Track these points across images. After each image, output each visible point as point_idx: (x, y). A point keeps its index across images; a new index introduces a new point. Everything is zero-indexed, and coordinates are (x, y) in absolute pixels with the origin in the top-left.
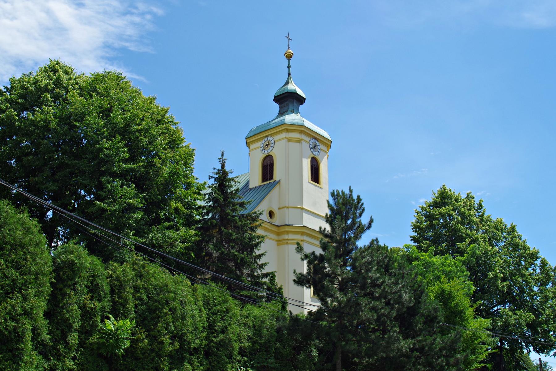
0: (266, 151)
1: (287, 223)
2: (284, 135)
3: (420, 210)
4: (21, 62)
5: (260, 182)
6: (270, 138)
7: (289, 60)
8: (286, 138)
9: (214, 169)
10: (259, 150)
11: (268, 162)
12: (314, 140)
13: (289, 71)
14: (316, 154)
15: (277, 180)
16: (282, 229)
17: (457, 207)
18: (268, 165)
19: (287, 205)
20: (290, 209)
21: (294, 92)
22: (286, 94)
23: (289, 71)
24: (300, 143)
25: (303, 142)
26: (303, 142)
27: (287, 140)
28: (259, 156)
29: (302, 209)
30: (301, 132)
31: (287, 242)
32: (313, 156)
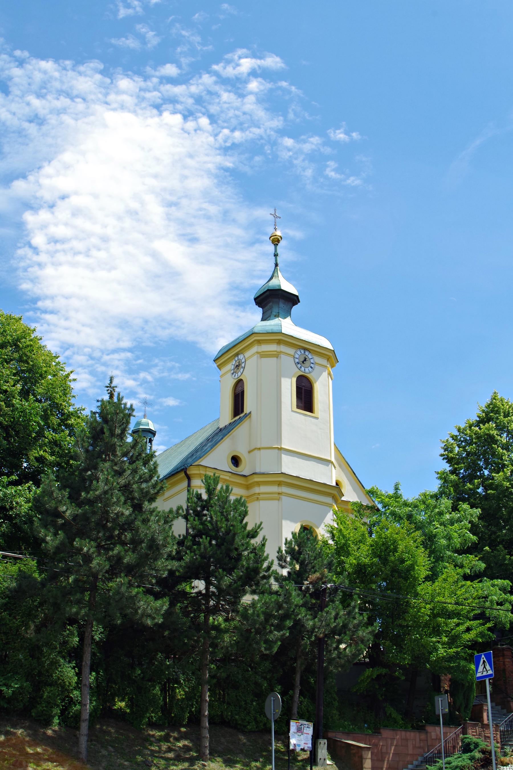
0: (237, 375)
1: (258, 471)
2: (255, 349)
3: (456, 433)
4: (128, 322)
5: (230, 419)
6: (241, 357)
7: (276, 245)
8: (257, 353)
9: (98, 401)
10: (229, 374)
11: (239, 389)
12: (303, 351)
13: (276, 260)
14: (307, 370)
15: (248, 412)
16: (251, 480)
17: (504, 423)
18: (239, 394)
19: (259, 446)
20: (262, 451)
21: (278, 288)
22: (268, 293)
23: (276, 260)
24: (277, 358)
25: (282, 356)
26: (282, 356)
27: (259, 355)
28: (230, 382)
29: (280, 449)
30: (279, 342)
31: (258, 498)
32: (302, 374)
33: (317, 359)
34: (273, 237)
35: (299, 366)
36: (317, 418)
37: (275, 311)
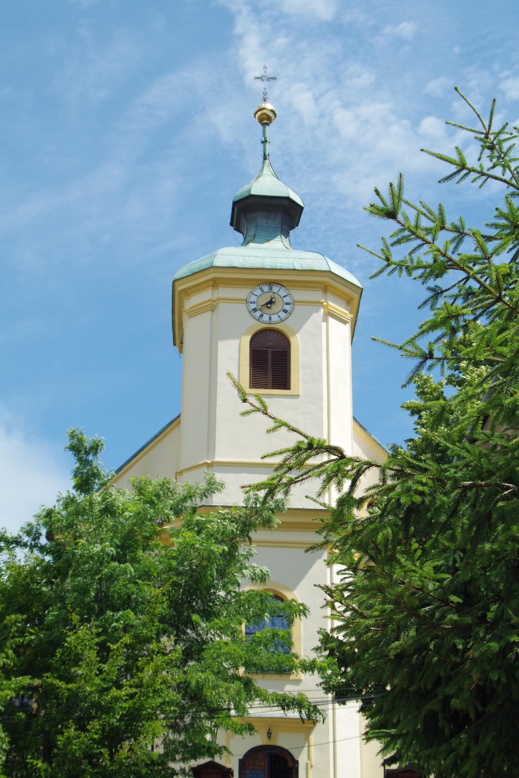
12: (266, 288)
14: (275, 318)
21: (246, 195)
24: (212, 311)
30: (215, 283)
33: (298, 295)
34: (259, 113)
35: (258, 314)
36: (297, 396)
37: (251, 233)
